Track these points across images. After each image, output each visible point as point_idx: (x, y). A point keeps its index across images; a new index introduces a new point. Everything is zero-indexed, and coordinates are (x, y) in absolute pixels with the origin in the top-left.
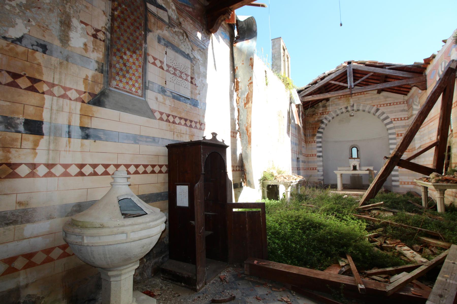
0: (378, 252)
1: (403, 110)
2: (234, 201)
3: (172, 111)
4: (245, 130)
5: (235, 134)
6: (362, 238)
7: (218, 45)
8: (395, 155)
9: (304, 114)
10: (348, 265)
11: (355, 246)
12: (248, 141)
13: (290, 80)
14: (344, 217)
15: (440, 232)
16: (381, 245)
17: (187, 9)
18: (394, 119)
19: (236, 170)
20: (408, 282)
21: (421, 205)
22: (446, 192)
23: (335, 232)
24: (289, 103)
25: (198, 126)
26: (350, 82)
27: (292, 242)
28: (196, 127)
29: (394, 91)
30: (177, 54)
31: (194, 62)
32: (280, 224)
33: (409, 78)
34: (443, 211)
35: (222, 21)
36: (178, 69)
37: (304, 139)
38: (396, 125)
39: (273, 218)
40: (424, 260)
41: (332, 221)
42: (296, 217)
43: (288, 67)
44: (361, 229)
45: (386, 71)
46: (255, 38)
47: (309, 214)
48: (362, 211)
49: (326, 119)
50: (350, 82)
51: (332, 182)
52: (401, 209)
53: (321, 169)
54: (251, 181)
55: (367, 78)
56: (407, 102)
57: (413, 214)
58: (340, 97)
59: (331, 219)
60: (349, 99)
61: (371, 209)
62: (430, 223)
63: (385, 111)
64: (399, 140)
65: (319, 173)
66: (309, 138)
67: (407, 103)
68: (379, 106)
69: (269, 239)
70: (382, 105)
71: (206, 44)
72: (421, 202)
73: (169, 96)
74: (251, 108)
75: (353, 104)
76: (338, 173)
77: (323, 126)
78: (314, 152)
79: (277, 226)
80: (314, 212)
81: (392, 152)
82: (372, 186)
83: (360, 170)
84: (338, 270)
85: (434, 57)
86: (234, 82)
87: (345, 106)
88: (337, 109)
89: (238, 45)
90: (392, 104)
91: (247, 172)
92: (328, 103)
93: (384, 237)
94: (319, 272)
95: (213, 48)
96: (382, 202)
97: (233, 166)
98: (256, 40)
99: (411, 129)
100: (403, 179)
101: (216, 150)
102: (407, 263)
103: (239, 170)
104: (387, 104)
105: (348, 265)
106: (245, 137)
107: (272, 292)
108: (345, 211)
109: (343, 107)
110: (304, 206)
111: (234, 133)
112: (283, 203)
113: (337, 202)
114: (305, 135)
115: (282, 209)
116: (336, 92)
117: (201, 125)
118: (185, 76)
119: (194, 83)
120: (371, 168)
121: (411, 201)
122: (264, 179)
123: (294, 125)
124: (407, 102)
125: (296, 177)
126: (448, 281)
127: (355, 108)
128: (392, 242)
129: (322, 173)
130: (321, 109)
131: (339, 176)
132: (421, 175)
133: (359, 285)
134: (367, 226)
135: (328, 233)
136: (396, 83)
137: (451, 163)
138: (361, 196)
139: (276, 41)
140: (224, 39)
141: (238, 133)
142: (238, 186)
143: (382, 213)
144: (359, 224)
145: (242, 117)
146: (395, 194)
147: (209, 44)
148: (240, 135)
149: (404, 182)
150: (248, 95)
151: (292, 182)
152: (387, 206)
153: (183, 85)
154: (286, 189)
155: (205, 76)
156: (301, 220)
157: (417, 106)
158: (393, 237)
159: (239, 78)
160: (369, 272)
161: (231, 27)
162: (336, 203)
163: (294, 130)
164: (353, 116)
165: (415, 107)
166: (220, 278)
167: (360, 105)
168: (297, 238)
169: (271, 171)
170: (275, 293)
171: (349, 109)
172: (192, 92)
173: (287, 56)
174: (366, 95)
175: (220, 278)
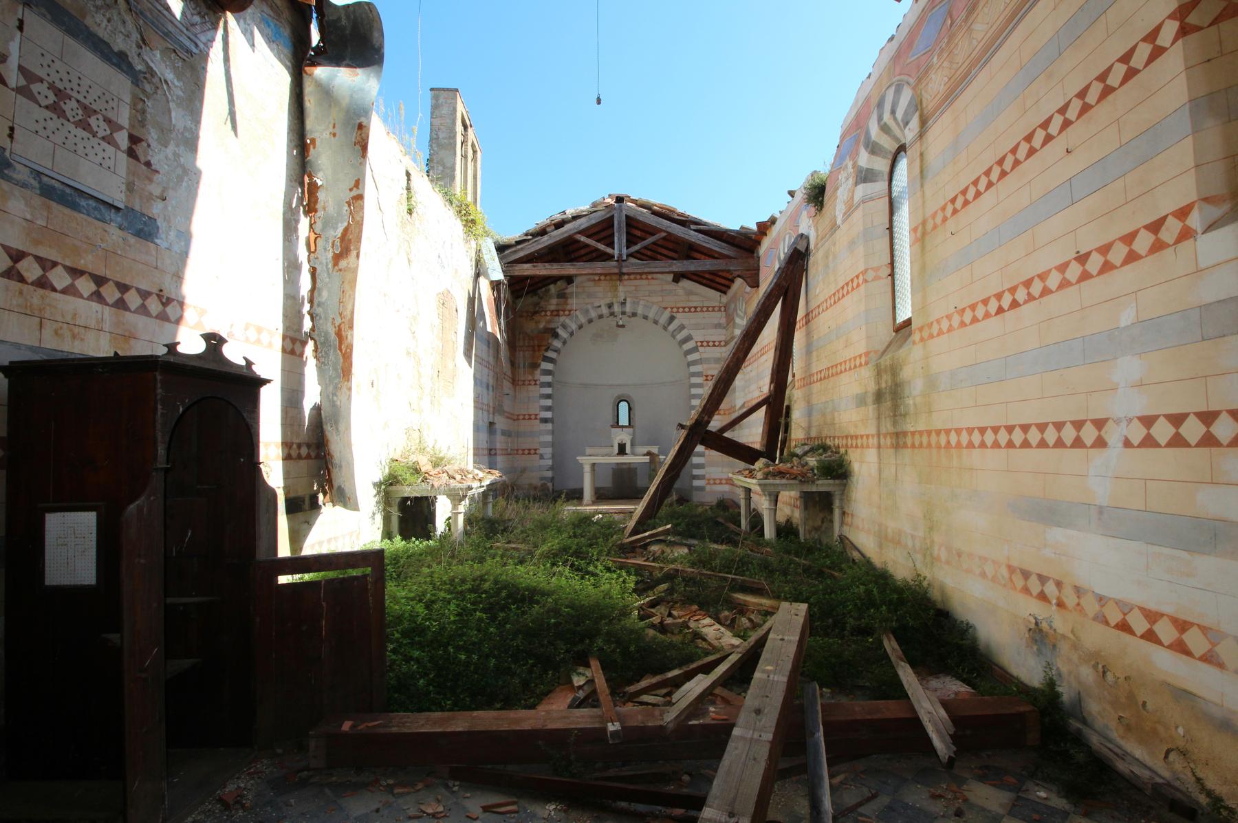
0: (654, 638)
1: (718, 326)
2: (284, 551)
3: (37, 242)
4: (333, 336)
5: (298, 344)
6: (625, 613)
10: (591, 682)
11: (608, 633)
12: (339, 366)
13: (478, 212)
14: (591, 568)
16: (661, 623)
19: (299, 457)
20: (707, 696)
21: (739, 526)
24: (471, 272)
25: (154, 306)
26: (619, 247)
28: (143, 310)
30: (70, 41)
31: (148, 87)
32: (428, 607)
34: (773, 535)
36: (74, 94)
37: (509, 373)
38: (705, 356)
40: (736, 641)
41: (564, 582)
42: (474, 580)
45: (692, 235)
46: (376, 67)
47: (510, 567)
49: (564, 326)
50: (620, 244)
51: (572, 485)
52: (702, 538)
53: (548, 451)
55: (654, 243)
56: (726, 307)
57: (724, 547)
59: (561, 574)
61: (648, 544)
63: (685, 322)
64: (706, 391)
65: (542, 462)
66: (521, 371)
69: (394, 651)
71: (203, 38)
73: (24, 185)
76: (586, 461)
77: (557, 344)
78: (534, 409)
79: (421, 611)
80: (521, 562)
81: (694, 414)
82: (652, 489)
83: (634, 454)
85: (773, 221)
86: (302, 184)
87: (608, 301)
88: (589, 307)
89: (321, 72)
91: (336, 459)
92: (572, 289)
94: (522, 713)
95: (226, 59)
97: (286, 444)
98: (378, 75)
100: (714, 474)
101: (222, 390)
102: (707, 654)
103: (308, 457)
105: (591, 682)
106: (332, 357)
107: (391, 799)
108: (594, 552)
109: (603, 303)
111: (293, 340)
112: (442, 546)
115: (439, 563)
116: (588, 264)
117: (165, 305)
118: (103, 124)
119: (143, 159)
120: (655, 450)
121: (723, 520)
123: (485, 336)
124: (726, 307)
125: (481, 475)
127: (628, 308)
128: (682, 613)
129: (550, 462)
130: (554, 301)
131: (587, 469)
132: (741, 465)
133: (610, 724)
134: (637, 583)
136: (706, 265)
139: (443, 97)
140: (270, 40)
141: (310, 347)
142: (303, 508)
143: (668, 550)
145: (325, 294)
146: (697, 506)
148: (316, 350)
150: (346, 230)
151: (470, 488)
152: (679, 534)
153: (92, 156)
154: (455, 507)
156: (486, 586)
158: (687, 601)
159: (320, 174)
162: (575, 536)
163: (485, 348)
164: (623, 326)
165: (738, 320)
166: (220, 800)
169: (413, 458)
170: (400, 801)
171: (617, 308)
172: (130, 187)
173: (473, 145)
175: (220, 800)
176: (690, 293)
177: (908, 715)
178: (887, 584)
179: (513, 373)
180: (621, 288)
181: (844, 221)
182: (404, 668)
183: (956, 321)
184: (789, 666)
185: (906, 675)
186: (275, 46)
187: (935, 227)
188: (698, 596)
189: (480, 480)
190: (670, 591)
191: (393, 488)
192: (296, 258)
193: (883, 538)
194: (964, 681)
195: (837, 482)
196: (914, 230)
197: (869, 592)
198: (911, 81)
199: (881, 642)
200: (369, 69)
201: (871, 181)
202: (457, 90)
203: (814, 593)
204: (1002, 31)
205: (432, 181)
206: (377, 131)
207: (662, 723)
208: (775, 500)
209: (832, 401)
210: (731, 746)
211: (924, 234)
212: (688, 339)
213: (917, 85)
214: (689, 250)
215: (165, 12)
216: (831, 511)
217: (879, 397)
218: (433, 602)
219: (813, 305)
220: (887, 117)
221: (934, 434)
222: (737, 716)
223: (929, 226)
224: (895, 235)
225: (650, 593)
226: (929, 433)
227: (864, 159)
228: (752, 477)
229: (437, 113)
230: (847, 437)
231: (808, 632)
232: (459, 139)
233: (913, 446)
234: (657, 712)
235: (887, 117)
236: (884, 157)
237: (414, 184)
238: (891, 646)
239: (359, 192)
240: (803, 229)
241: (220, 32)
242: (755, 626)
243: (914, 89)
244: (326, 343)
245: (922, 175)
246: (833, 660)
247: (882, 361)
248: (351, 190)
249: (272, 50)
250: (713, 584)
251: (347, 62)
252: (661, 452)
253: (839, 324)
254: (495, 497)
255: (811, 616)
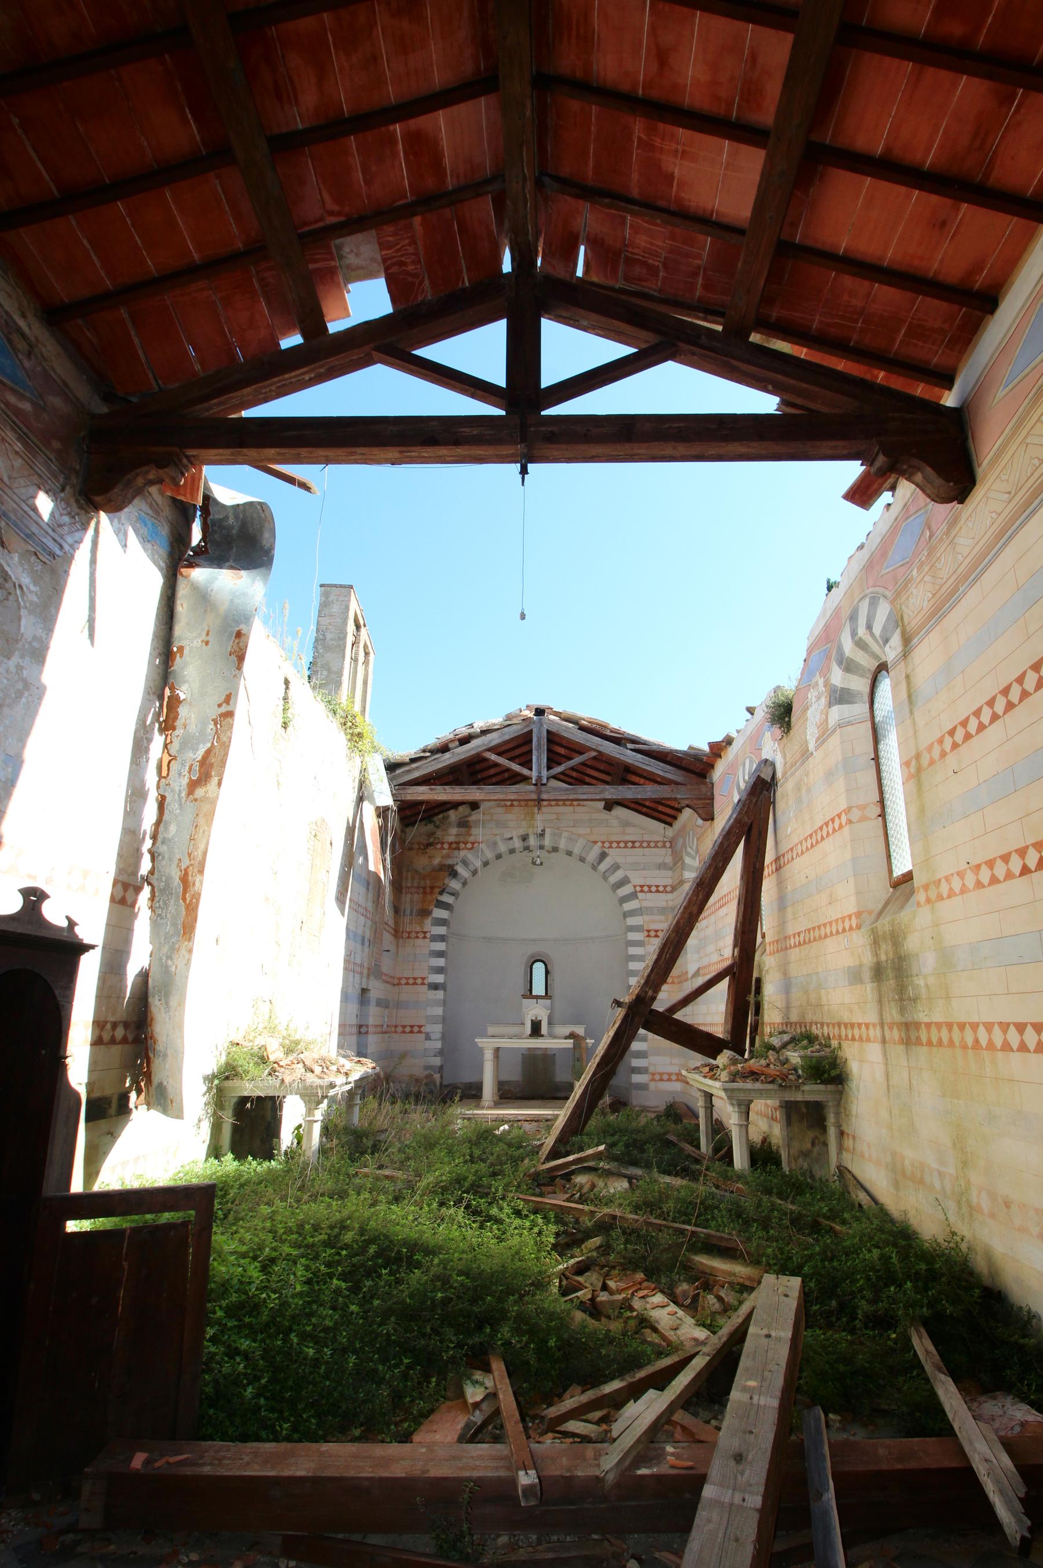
1: (662, 866)
2: (77, 1186)
4: (176, 881)
6: (540, 1284)
7: (115, 565)
8: (638, 996)
9: (400, 840)
13: (367, 724)
14: (494, 1211)
15: (738, 1236)
16: (592, 1299)
17: (12, 399)
18: (642, 886)
19: (113, 1041)
21: (698, 1147)
22: (752, 1106)
23: (461, 1273)
24: (353, 796)
27: (304, 1337)
29: (644, 810)
33: (677, 783)
34: (746, 1165)
35: (151, 483)
37: (391, 923)
38: (645, 904)
39: (242, 1241)
40: (701, 1334)
41: (453, 1231)
42: (332, 1228)
43: (365, 683)
44: (539, 1246)
45: (627, 755)
46: (262, 570)
48: (544, 1182)
49: (465, 863)
51: (468, 1078)
52: (648, 1166)
53: (436, 1030)
54: (170, 1085)
55: (583, 764)
56: (672, 842)
58: (509, 803)
60: (533, 814)
61: (573, 1172)
62: (717, 1207)
63: (620, 860)
64: (652, 948)
65: (428, 1044)
66: (407, 919)
67: (671, 847)
68: (607, 845)
69: (214, 1340)
70: (615, 845)
71: (70, 539)
72: (698, 1139)
74: (213, 802)
75: (543, 830)
76: (487, 1045)
77: (454, 885)
80: (397, 1199)
81: (635, 982)
82: (579, 1088)
84: (461, 1422)
85: (729, 741)
87: (522, 832)
88: (498, 839)
89: (200, 575)
90: (637, 844)
91: (160, 1047)
92: (475, 816)
93: (603, 1267)
94: (394, 1449)
95: (93, 561)
96: (602, 1148)
97: (98, 1024)
98: (265, 578)
99: (678, 922)
100: (661, 1069)
102: (660, 1354)
103: (124, 1041)
104: (626, 842)
105: (492, 1396)
106: (172, 908)
108: (498, 1186)
109: (516, 833)
110: (366, 1176)
111: (126, 886)
113: (477, 1152)
114: (396, 910)
115: (284, 1199)
120: (580, 1030)
121: (673, 1140)
122: (229, 1072)
123: (364, 875)
124: (672, 842)
125: (348, 1065)
126: (756, 1398)
127: (547, 842)
129: (438, 1045)
130: (454, 831)
131: (489, 1055)
132: (697, 1059)
133: (521, 1473)
134: (557, 1235)
135: (437, 1278)
136: (647, 792)
137: (763, 1024)
138: (549, 1121)
139: (334, 595)
140: (144, 540)
141: (146, 891)
142: (108, 1111)
143: (600, 1183)
144: (536, 1230)
145: (173, 829)
147: (81, 541)
148: (152, 898)
149: (661, 1074)
150: (208, 752)
151: (332, 1086)
152: (615, 1159)
154: (310, 1112)
155: (39, 654)
156: (348, 1237)
157: (694, 858)
158: (630, 1265)
159: (185, 687)
160: (553, 1412)
161: (183, 513)
165: (688, 860)
167: (560, 835)
168: (328, 1317)
169: (260, 1041)
171: (532, 841)
173: (365, 646)
174: (578, 809)
176: (626, 824)
177: (955, 1464)
178: (910, 1246)
179: (396, 923)
180: (539, 817)
181: (817, 748)
182: (226, 1368)
183: (970, 880)
184: (779, 1381)
185: (949, 1395)
186: (149, 546)
187: (932, 762)
188: (644, 1258)
189: (346, 1074)
190: (605, 1249)
191: (229, 1084)
192: (143, 784)
193: (899, 1174)
194: (1032, 1404)
195: (830, 1087)
196: (906, 764)
197: (885, 1259)
198: (888, 594)
199: (909, 1339)
200: (254, 572)
201: (848, 702)
202: (351, 587)
203: (810, 1257)
204: (990, 548)
205: (314, 688)
206: (260, 644)
207: (597, 1472)
208: (745, 1109)
209: (818, 976)
210: (702, 1514)
211: (919, 770)
212: (624, 881)
213: (895, 599)
214: (625, 774)
215: (31, 513)
216: (824, 1129)
217: (878, 972)
218: (273, 1261)
219: (784, 847)
220: (862, 631)
221: (955, 1028)
222: (707, 1462)
223: (925, 760)
224: (883, 768)
225: (576, 1251)
226: (950, 1026)
227: (838, 677)
228: (713, 1077)
229: (326, 611)
230: (839, 1024)
231: (803, 1324)
232: (350, 639)
233: (930, 1043)
234: (590, 1450)
235: (862, 631)
236: (862, 676)
237: (291, 693)
238: (922, 1345)
239: (229, 708)
240: (767, 753)
241: (91, 532)
242: (727, 1309)
243: (892, 602)
244: (167, 890)
245: (910, 699)
246: (841, 1368)
247: (879, 924)
248: (220, 706)
249: (145, 550)
250: (665, 1238)
251: (231, 563)
252: (589, 1034)
253: (818, 874)
254: (363, 1097)
255: (805, 1294)
